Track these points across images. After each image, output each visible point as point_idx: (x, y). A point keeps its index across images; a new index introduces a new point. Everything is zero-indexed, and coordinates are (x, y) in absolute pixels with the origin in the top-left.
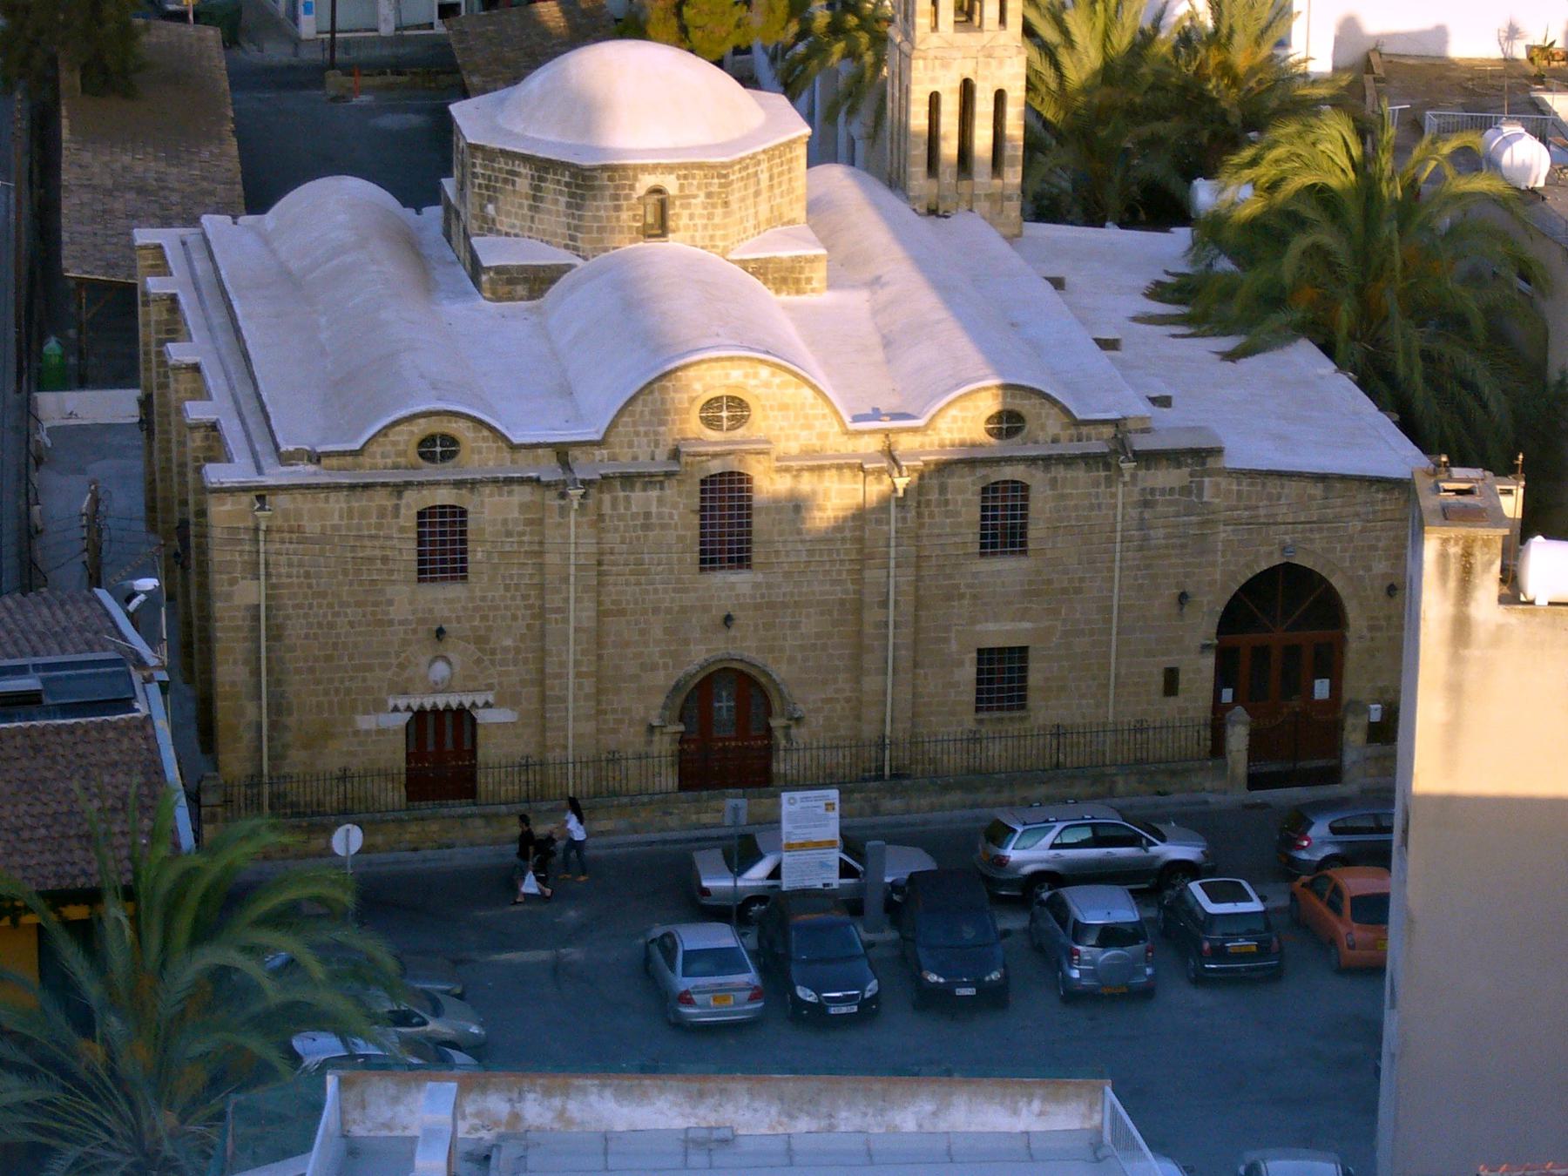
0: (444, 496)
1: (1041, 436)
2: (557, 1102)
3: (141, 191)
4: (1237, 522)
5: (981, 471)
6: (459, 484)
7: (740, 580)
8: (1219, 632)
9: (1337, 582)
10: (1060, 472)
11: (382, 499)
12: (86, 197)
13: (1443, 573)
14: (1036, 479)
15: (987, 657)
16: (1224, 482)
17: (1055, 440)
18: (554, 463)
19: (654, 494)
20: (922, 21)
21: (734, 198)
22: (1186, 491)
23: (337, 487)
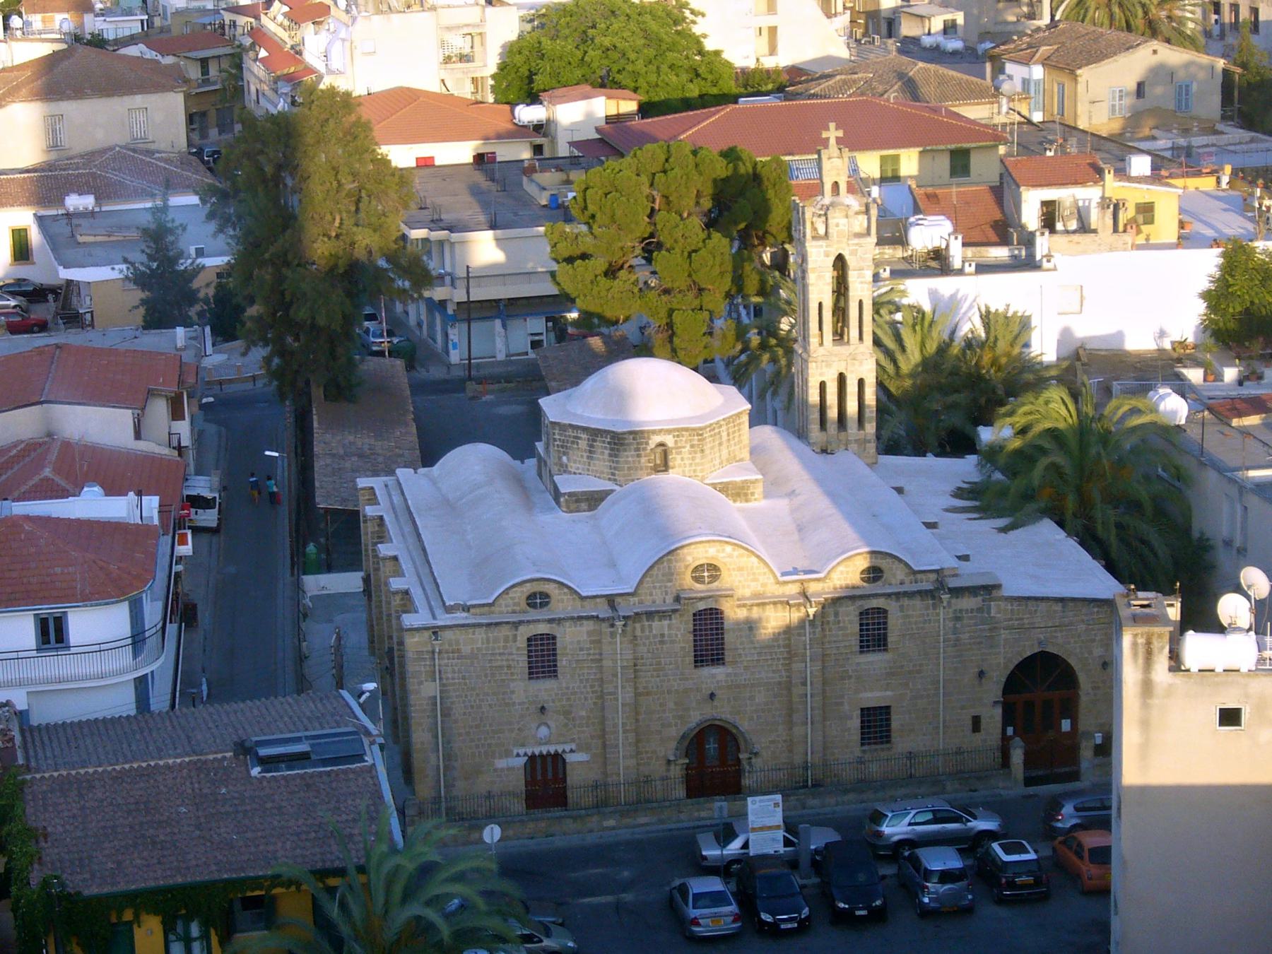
0: (543, 629)
3: (361, 456)
5: (860, 603)
6: (551, 621)
8: (1004, 694)
10: (906, 602)
11: (506, 631)
13: (1135, 654)
14: (891, 606)
15: (866, 712)
18: (606, 607)
19: (666, 622)
20: (814, 341)
21: (707, 447)
22: (980, 610)
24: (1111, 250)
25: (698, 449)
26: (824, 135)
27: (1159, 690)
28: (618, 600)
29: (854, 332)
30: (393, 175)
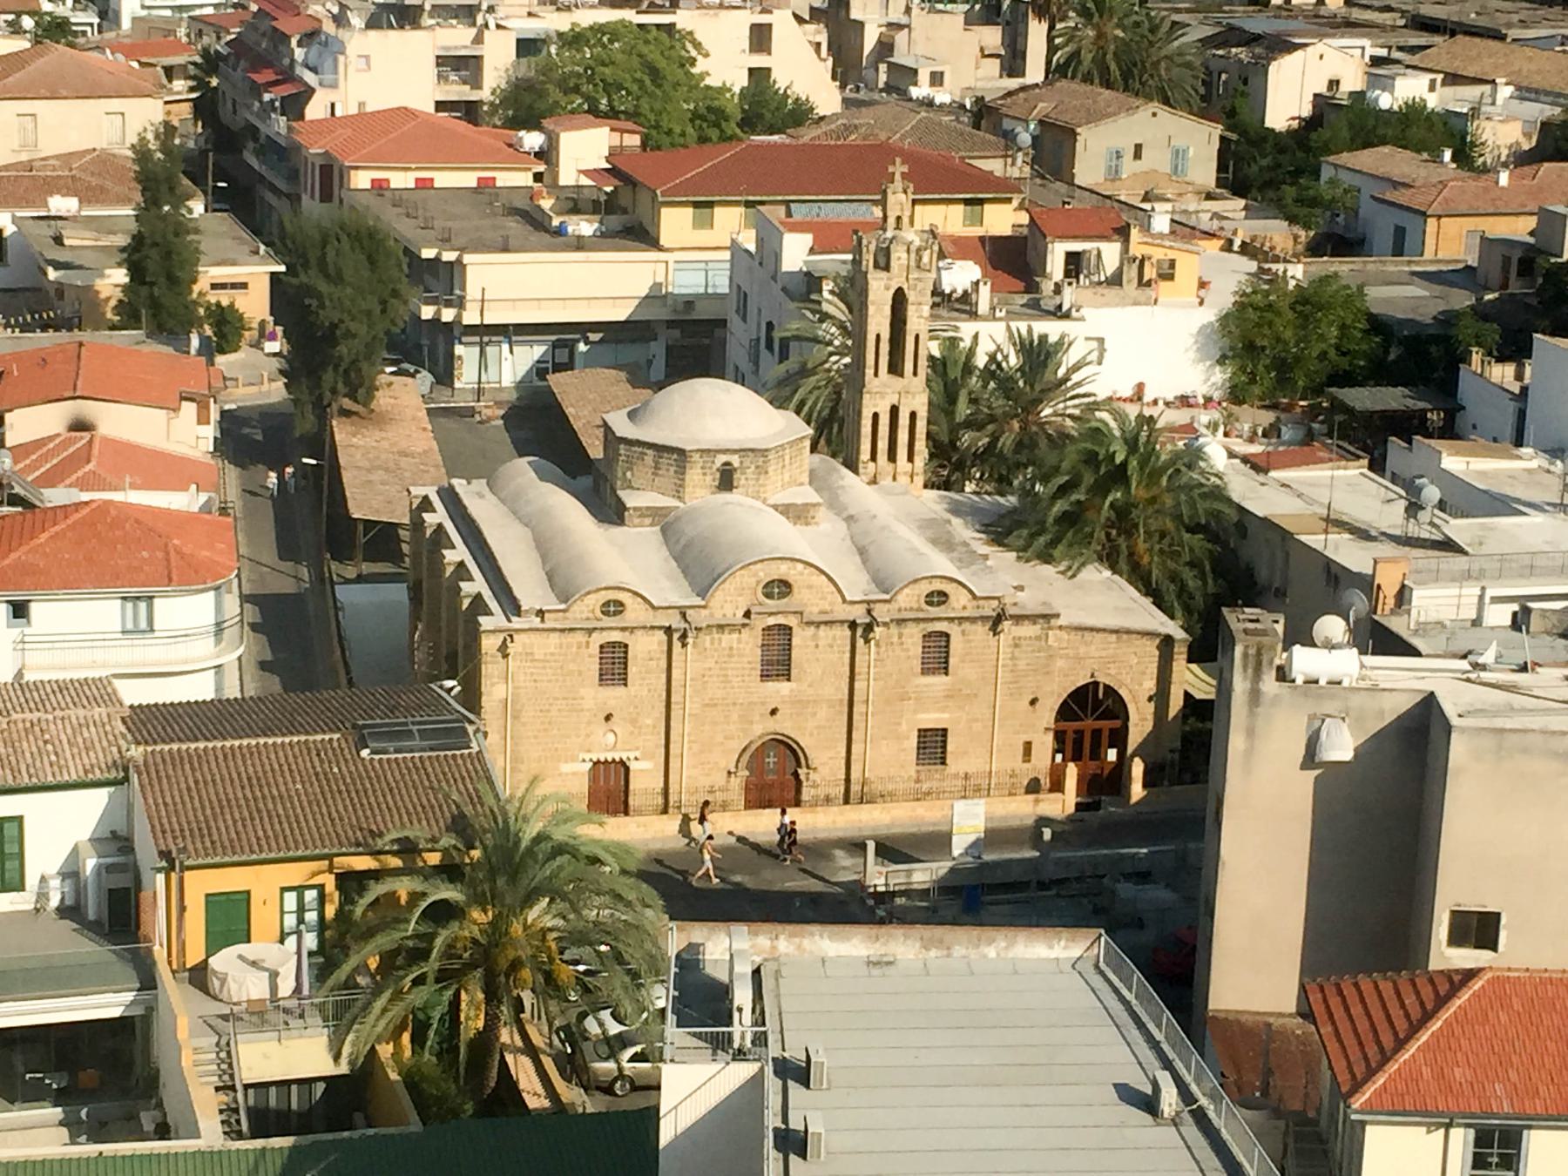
0: (616, 636)
1: (955, 605)
2: (797, 940)
3: (387, 470)
4: (1067, 657)
5: (922, 625)
6: (623, 629)
7: (783, 687)
8: (1057, 721)
9: (1123, 692)
10: (966, 625)
11: (580, 637)
12: (356, 473)
13: (1245, 667)
14: (953, 630)
15: (923, 733)
16: (1064, 635)
17: (964, 608)
18: (679, 617)
19: (735, 636)
20: (869, 372)
21: (770, 469)
22: (1038, 638)
23: (554, 630)
24: (1136, 303)
25: (762, 471)
26: (891, 169)
27: (1265, 700)
28: (689, 612)
29: (909, 366)
30: (1431, 128)
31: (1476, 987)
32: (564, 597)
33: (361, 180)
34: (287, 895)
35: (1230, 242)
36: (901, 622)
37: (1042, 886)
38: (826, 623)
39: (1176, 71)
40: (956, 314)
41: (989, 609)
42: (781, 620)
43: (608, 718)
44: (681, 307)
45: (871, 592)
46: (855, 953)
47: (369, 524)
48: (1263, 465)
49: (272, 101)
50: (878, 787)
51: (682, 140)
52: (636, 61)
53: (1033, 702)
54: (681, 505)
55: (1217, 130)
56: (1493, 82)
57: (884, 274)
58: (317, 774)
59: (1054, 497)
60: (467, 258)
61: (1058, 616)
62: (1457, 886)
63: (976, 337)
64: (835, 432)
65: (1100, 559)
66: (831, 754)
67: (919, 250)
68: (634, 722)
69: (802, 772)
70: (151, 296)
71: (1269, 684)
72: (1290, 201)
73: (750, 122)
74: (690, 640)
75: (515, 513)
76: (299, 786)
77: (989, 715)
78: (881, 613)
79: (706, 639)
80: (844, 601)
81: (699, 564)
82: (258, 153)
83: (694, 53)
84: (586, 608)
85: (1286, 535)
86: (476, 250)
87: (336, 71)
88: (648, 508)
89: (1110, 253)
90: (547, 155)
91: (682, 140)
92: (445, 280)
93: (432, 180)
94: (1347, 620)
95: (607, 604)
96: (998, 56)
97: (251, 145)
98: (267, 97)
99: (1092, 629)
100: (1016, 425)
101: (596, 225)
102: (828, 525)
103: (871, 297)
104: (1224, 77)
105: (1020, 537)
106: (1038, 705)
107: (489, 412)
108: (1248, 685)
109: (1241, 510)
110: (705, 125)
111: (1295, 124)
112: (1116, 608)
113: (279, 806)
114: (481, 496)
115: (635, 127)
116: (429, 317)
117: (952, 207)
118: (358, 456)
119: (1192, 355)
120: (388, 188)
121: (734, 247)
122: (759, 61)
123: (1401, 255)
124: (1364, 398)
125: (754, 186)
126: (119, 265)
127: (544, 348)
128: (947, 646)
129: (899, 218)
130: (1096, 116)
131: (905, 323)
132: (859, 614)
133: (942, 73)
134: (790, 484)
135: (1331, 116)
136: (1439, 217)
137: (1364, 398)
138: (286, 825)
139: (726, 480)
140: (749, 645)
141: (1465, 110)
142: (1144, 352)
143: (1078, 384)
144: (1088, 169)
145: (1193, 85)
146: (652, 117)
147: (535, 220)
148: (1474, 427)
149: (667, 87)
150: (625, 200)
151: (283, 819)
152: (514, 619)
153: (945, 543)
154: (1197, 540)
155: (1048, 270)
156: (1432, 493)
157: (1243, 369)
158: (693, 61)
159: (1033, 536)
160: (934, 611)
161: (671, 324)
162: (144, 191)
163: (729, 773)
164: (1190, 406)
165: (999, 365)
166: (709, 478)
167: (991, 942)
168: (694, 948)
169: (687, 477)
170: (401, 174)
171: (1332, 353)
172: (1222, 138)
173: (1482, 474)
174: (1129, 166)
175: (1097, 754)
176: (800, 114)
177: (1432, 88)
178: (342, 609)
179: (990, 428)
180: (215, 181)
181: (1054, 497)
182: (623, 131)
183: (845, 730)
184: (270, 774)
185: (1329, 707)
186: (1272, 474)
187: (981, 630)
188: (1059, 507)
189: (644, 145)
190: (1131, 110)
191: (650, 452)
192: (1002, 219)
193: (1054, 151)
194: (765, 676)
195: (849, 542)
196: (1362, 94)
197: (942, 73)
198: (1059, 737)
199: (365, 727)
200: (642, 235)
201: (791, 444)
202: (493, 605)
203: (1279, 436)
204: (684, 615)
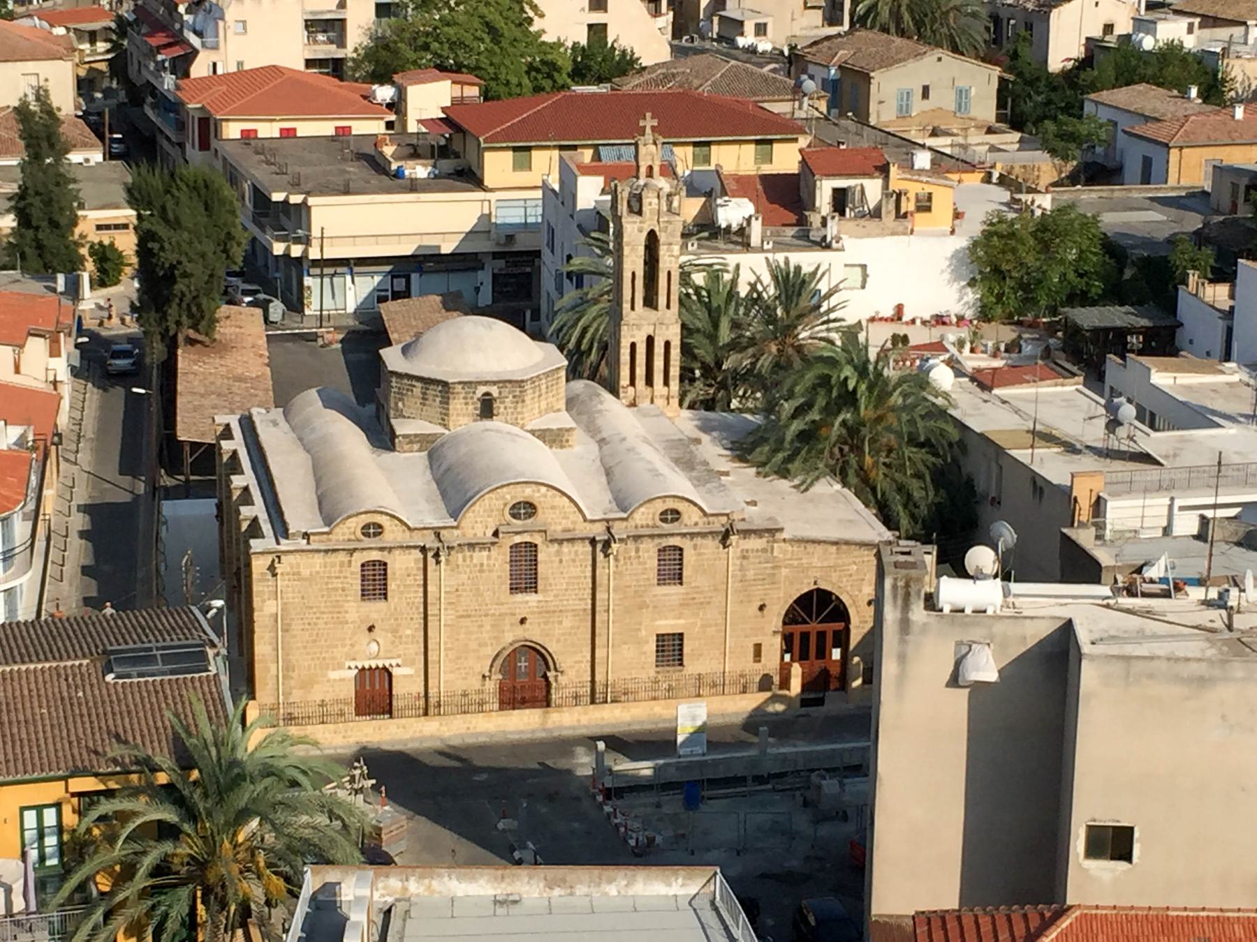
0: (375, 556)
2: (426, 881)
3: (219, 395)
4: (791, 566)
5: (657, 541)
6: (382, 549)
7: (531, 598)
8: (784, 623)
10: (698, 541)
11: (342, 557)
13: (895, 597)
15: (660, 638)
17: (696, 524)
19: (485, 553)
20: (626, 306)
21: (528, 399)
22: (764, 550)
23: (318, 551)
24: (893, 234)
27: (915, 629)
28: (443, 532)
29: (662, 300)
31: (1064, 926)
32: (329, 520)
33: (232, 130)
34: (26, 813)
35: (990, 175)
36: (637, 538)
37: (759, 779)
38: (568, 540)
39: (963, 20)
40: (731, 246)
41: (718, 525)
42: (526, 538)
43: (371, 629)
44: (503, 241)
45: (611, 511)
46: (482, 893)
47: (195, 446)
48: (988, 383)
49: (163, 61)
50: (620, 687)
51: (518, 90)
52: (476, 23)
53: (762, 608)
54: (447, 432)
55: (996, 72)
56: (1245, 23)
57: (636, 218)
58: (62, 699)
59: (794, 416)
60: (311, 201)
61: (781, 530)
62: (1090, 806)
63: (738, 267)
64: (592, 362)
65: (833, 472)
66: (578, 658)
67: (669, 195)
68: (394, 631)
69: (551, 675)
70: (36, 240)
71: (918, 613)
72: (1051, 136)
73: (580, 73)
74: (443, 558)
75: (301, 439)
76: (44, 711)
77: (721, 621)
78: (619, 530)
79: (458, 557)
80: (585, 520)
81: (454, 489)
82: (154, 106)
83: (531, 14)
84: (349, 529)
85: (999, 451)
86: (322, 193)
87: (217, 36)
88: (416, 435)
89: (873, 188)
90: (397, 106)
91: (518, 90)
92: (292, 219)
93: (294, 130)
94: (996, 551)
95: (367, 526)
96: (819, 8)
97: (150, 100)
98: (160, 58)
99: (814, 542)
100: (774, 349)
101: (430, 169)
102: (582, 447)
103: (625, 240)
104: (1012, 22)
105: (761, 453)
106: (766, 611)
107: (328, 337)
108: (898, 615)
109: (964, 427)
110: (540, 76)
111: (1070, 65)
112: (840, 521)
113: (23, 730)
114: (275, 424)
115: (477, 80)
116: (281, 253)
117: (744, 147)
118: (196, 383)
119: (947, 276)
120: (256, 138)
121: (545, 187)
122: (598, 18)
123: (1149, 183)
124: (1089, 317)
125: (565, 131)
126: (8, 211)
127: (377, 279)
128: (681, 560)
129: (651, 168)
130: (888, 62)
131: (657, 261)
132: (598, 531)
133: (765, 25)
134: (547, 411)
135: (1100, 57)
136: (1181, 148)
137: (1089, 317)
138: (26, 749)
139: (487, 409)
140: (498, 562)
141: (1218, 50)
142: (896, 277)
143: (830, 310)
144: (882, 111)
145: (980, 34)
146: (491, 70)
147: (377, 164)
148: (1191, 342)
149: (505, 44)
150: (457, 146)
151: (26, 742)
152: (283, 541)
153: (686, 460)
154: (919, 455)
155: (817, 204)
156: (1128, 411)
157: (991, 290)
158: (530, 21)
159: (775, 451)
160: (668, 528)
161: (496, 255)
162: (28, 146)
163: (484, 677)
164: (944, 323)
165: (759, 294)
166: (471, 407)
167: (610, 881)
168: (330, 889)
169: (451, 407)
170: (268, 124)
171: (1071, 276)
172: (1001, 80)
173: (1188, 388)
174: (918, 106)
175: (822, 653)
176: (626, 64)
177: (1190, 30)
178: (165, 523)
179: (751, 351)
180: (111, 133)
181: (794, 416)
182: (462, 83)
183: (589, 636)
184: (19, 699)
185: (976, 633)
186: (996, 391)
187: (712, 545)
188: (796, 426)
189: (487, 95)
190: (918, 55)
191: (419, 385)
192: (786, 159)
193: (849, 92)
194: (514, 589)
195: (599, 463)
196: (1128, 36)
197: (765, 25)
198: (788, 639)
199: (113, 652)
200: (470, 177)
201: (547, 375)
202: (266, 527)
203: (1020, 351)
204: (438, 535)
